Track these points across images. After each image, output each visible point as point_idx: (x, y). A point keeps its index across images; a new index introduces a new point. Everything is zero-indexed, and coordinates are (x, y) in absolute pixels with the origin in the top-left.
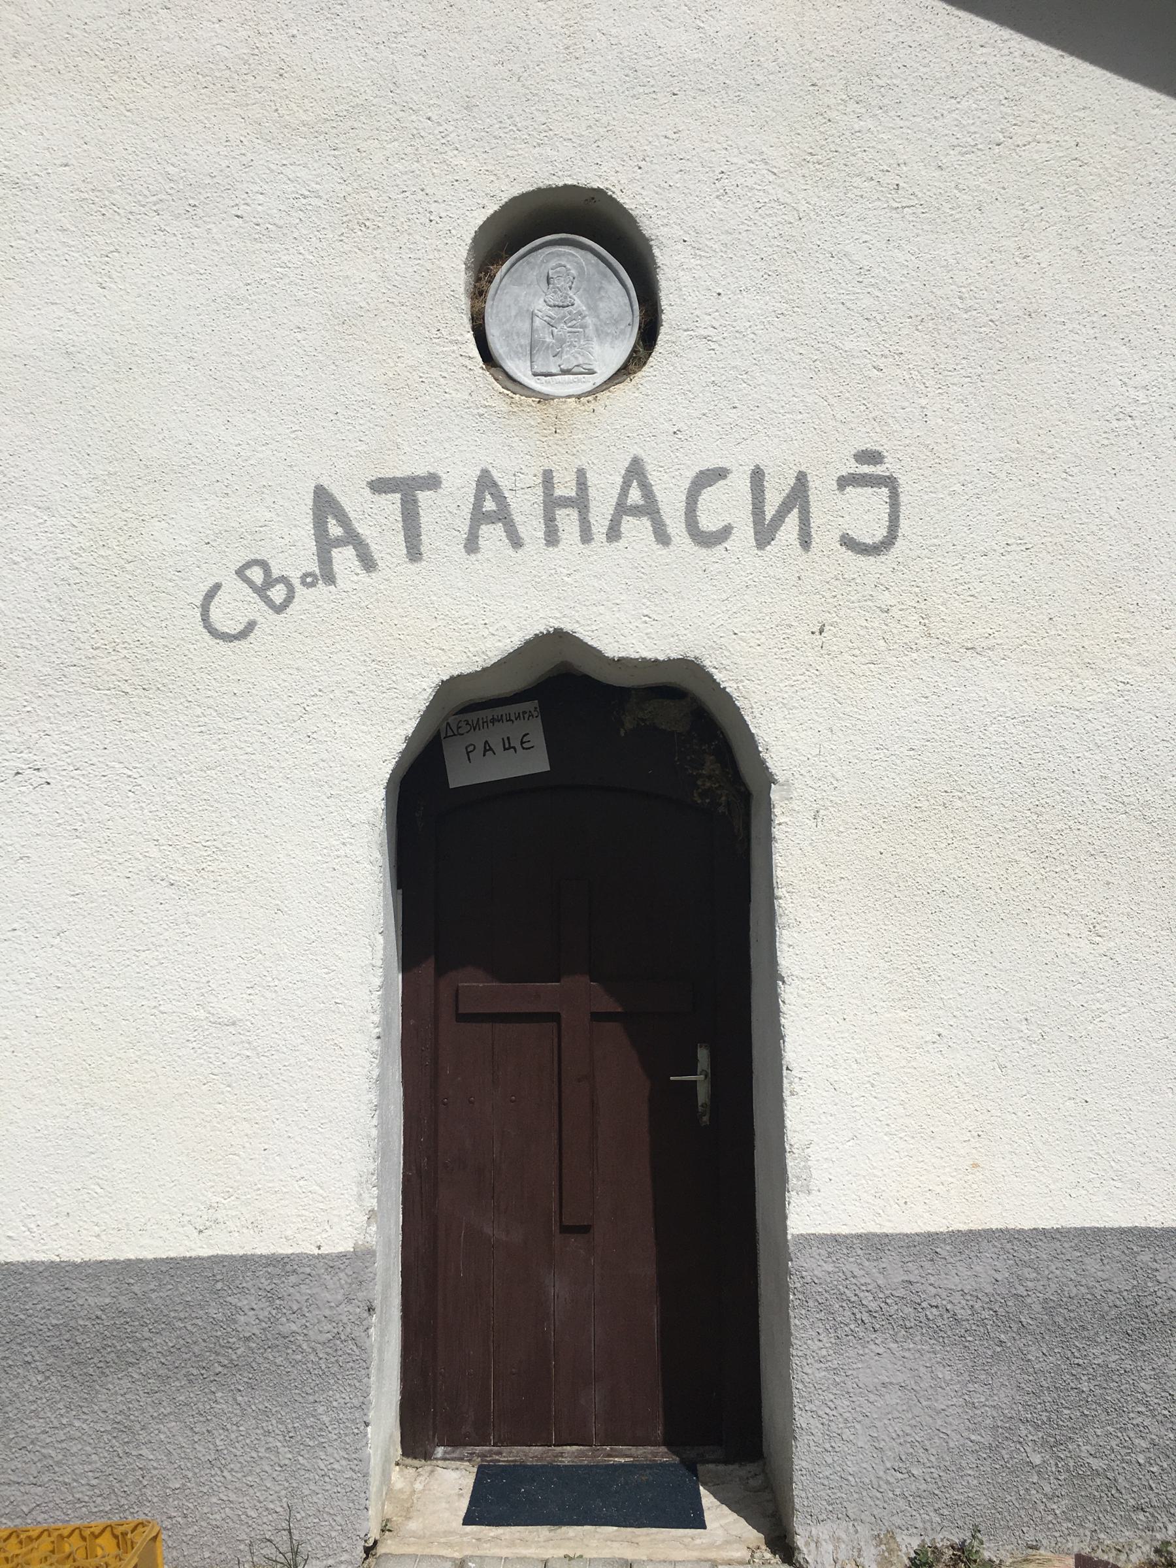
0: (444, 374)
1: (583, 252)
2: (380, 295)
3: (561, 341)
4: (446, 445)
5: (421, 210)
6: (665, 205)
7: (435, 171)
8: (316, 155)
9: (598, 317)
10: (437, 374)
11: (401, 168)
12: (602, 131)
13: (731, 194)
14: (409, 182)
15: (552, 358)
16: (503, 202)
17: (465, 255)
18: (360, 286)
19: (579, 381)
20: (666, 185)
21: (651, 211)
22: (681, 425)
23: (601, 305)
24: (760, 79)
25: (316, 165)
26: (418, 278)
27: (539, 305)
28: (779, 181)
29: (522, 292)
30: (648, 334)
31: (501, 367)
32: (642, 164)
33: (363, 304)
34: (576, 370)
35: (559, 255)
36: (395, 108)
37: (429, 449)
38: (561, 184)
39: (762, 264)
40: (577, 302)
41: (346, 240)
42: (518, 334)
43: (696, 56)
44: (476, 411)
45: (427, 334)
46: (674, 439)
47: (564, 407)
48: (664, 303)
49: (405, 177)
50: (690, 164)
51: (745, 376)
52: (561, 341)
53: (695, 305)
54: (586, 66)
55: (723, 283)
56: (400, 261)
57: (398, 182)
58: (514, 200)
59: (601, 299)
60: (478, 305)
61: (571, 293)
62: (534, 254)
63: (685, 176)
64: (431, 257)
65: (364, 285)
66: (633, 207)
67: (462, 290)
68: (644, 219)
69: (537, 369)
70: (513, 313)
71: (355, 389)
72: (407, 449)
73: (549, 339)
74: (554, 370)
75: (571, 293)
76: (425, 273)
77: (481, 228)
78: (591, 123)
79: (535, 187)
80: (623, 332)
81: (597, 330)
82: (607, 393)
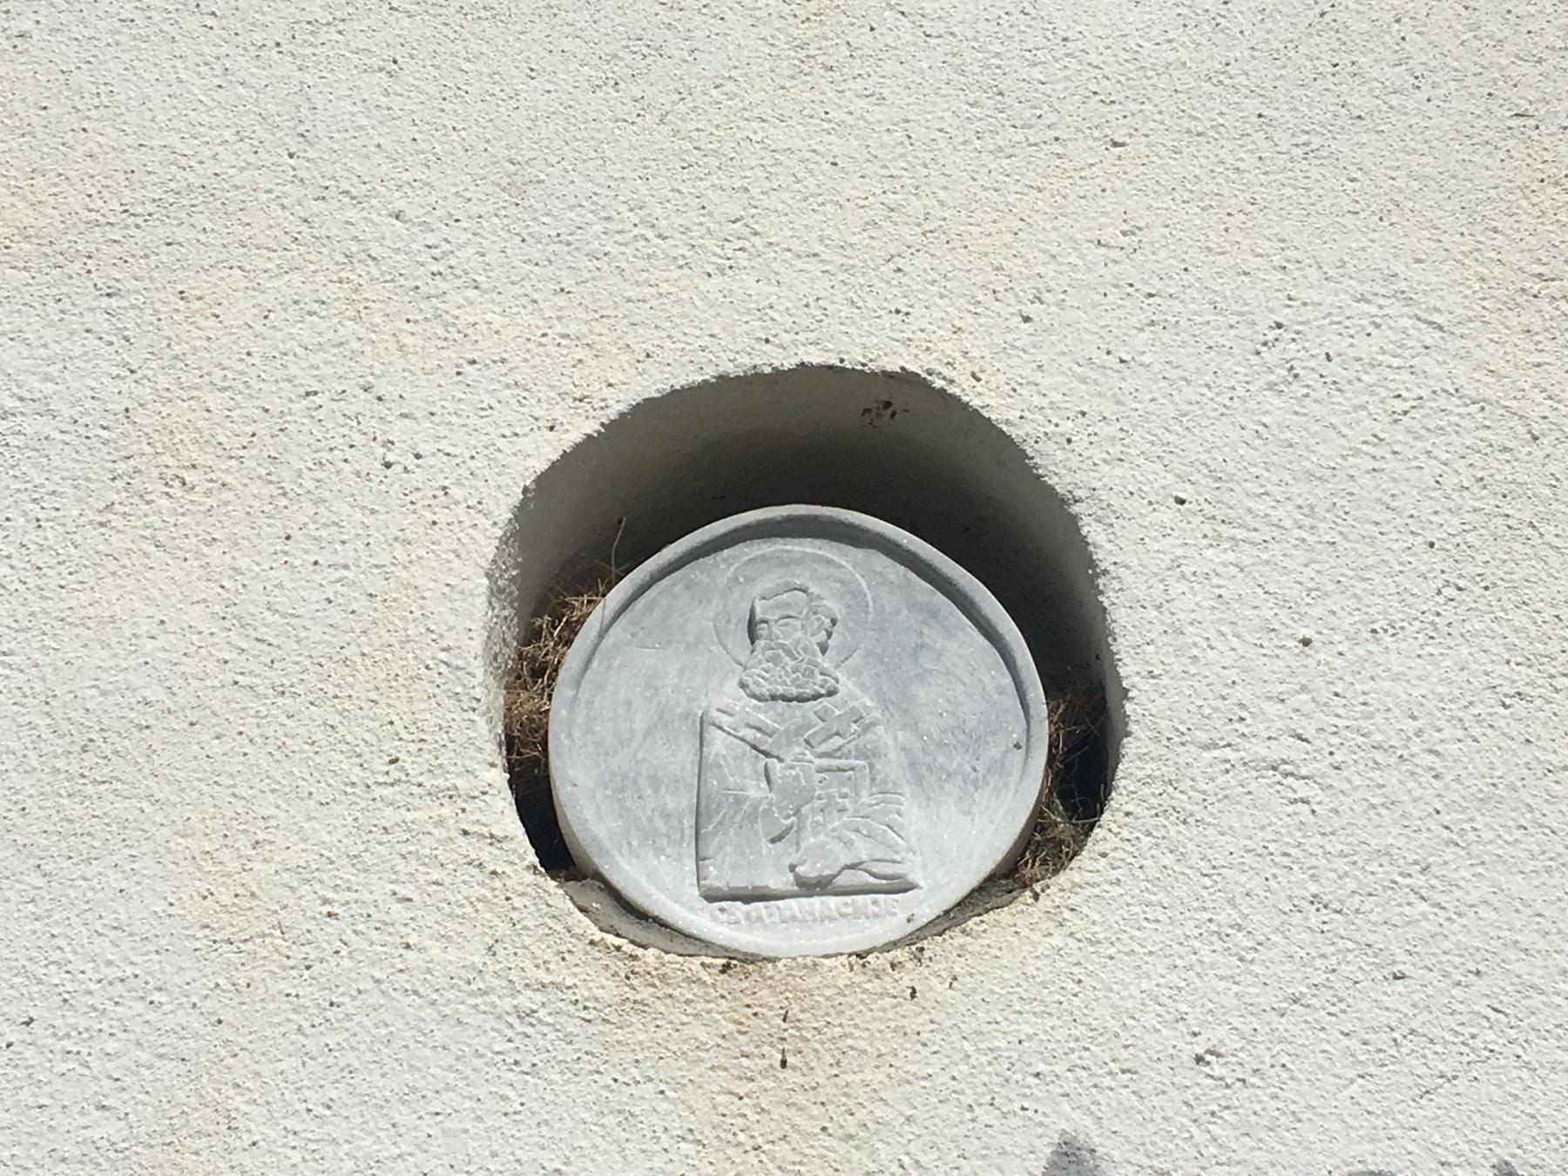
0: (403, 891)
1: (860, 554)
2: (211, 666)
3: (798, 798)
4: (401, 1115)
5: (358, 439)
6: (1109, 409)
7: (408, 340)
8: (53, 308)
9: (914, 728)
10: (382, 889)
11: (307, 337)
12: (909, 234)
13: (1310, 378)
14: (327, 370)
15: (766, 846)
16: (612, 413)
17: (490, 551)
18: (150, 645)
19: (858, 913)
20: (1112, 361)
21: (1066, 427)
22: (1216, 1034)
23: (922, 694)
24: (1360, 101)
25: (48, 333)
26: (334, 614)
27: (725, 698)
28: (1454, 345)
29: (675, 663)
30: (1082, 775)
31: (598, 877)
32: (1029, 309)
33: (155, 693)
34: (847, 879)
35: (782, 562)
36: (296, 192)
37: (337, 1129)
38: (789, 363)
39: (1436, 557)
40: (846, 685)
41: (119, 522)
42: (655, 782)
43: (1172, 56)
44: (507, 1004)
45: (356, 774)
46: (1199, 1076)
47: (812, 982)
48: (1129, 669)
49: (315, 359)
50: (1177, 307)
51: (1419, 881)
52: (798, 798)
53: (1232, 675)
54: (858, 85)
55: (1317, 611)
56: (282, 574)
57: (293, 370)
58: (647, 409)
59: (922, 677)
60: (528, 703)
61: (825, 662)
62: (709, 560)
63: (1166, 337)
64: (385, 559)
65: (162, 641)
66: (1013, 415)
67: (477, 645)
68: (1047, 447)
69: (718, 877)
70: (640, 723)
71: (104, 947)
72: (261, 1131)
73: (756, 791)
74: (778, 881)
75: (825, 662)
76: (361, 604)
77: (541, 479)
78: (877, 214)
79: (709, 373)
80: (998, 768)
81: (913, 765)
82: (956, 938)
